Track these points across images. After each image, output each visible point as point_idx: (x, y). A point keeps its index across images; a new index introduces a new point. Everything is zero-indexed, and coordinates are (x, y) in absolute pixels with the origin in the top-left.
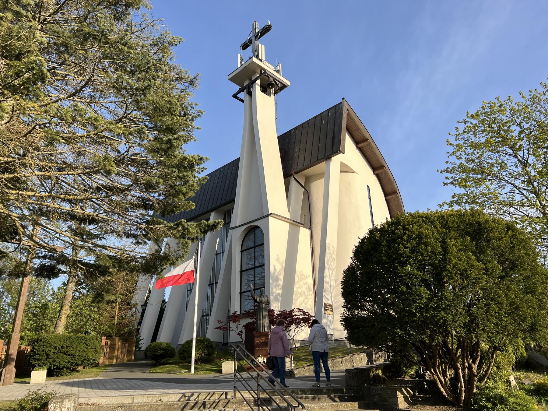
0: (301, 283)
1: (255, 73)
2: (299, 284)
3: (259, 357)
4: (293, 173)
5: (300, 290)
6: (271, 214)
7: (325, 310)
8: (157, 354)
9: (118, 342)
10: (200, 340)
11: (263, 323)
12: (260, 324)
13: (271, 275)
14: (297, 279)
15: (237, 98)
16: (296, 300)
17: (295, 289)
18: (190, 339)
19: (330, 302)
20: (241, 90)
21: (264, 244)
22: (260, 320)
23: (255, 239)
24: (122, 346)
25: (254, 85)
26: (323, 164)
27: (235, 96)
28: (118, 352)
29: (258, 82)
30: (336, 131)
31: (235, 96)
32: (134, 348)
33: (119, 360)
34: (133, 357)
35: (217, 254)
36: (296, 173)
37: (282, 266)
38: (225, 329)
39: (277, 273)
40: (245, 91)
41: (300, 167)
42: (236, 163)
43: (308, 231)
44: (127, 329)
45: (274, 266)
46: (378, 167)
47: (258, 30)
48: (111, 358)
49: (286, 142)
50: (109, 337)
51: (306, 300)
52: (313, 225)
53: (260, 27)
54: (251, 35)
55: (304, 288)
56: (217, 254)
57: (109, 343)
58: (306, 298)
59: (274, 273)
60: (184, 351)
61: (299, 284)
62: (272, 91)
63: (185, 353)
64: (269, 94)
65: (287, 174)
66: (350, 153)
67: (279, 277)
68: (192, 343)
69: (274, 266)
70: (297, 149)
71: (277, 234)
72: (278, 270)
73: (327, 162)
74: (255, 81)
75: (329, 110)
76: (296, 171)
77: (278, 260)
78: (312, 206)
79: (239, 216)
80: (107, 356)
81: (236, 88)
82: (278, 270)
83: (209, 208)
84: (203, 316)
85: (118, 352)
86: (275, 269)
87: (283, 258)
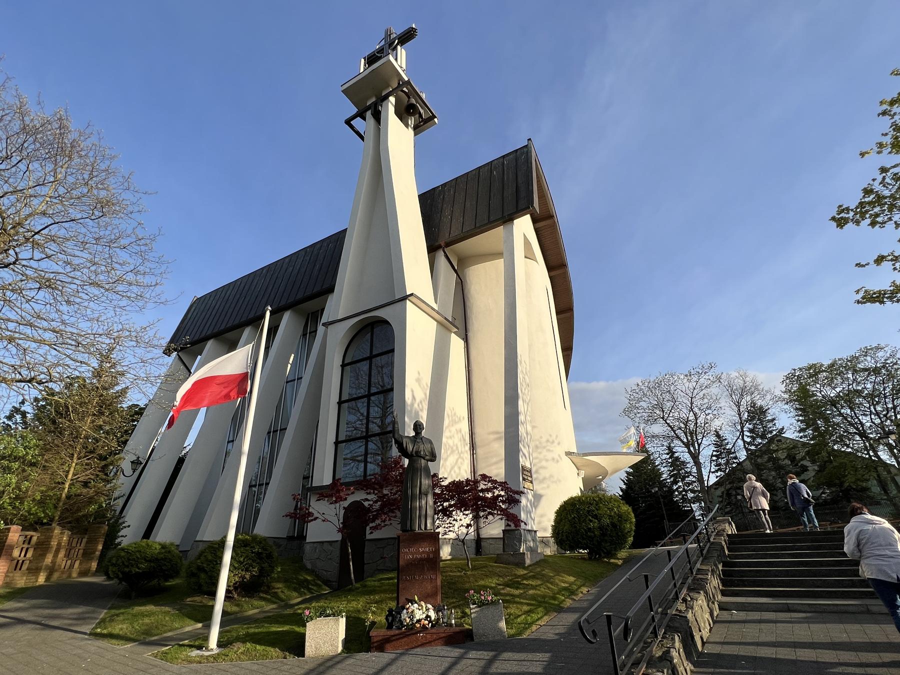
0: (453, 429)
1: (388, 86)
2: (450, 431)
3: (413, 602)
4: (443, 244)
5: (450, 442)
6: (412, 295)
7: (524, 479)
8: (135, 570)
9: (60, 536)
10: (243, 541)
11: (420, 507)
12: (412, 509)
13: (408, 408)
14: (446, 422)
15: (352, 127)
16: (446, 460)
17: (444, 440)
18: (218, 538)
19: (528, 465)
20: (361, 115)
21: (393, 351)
22: (413, 497)
23: (376, 342)
24: (70, 542)
25: (384, 104)
26: (500, 230)
27: (348, 122)
28: (56, 555)
29: (392, 99)
30: (520, 181)
31: (348, 122)
32: (100, 547)
33: (56, 576)
34: (94, 565)
35: (287, 382)
36: (448, 245)
37: (425, 394)
38: (300, 516)
39: (416, 405)
40: (369, 114)
41: (455, 232)
42: (337, 241)
43: (461, 343)
44: (93, 508)
45: (412, 391)
46: (557, 267)
47: (393, 36)
48: (34, 571)
49: (429, 202)
50: (30, 524)
51: (460, 460)
52: (470, 334)
53: (397, 31)
54: (383, 43)
55: (456, 440)
56: (287, 382)
57: (35, 539)
58: (460, 457)
59: (412, 405)
60: (201, 569)
61: (450, 431)
62: (411, 121)
63: (203, 576)
64: (407, 125)
65: (432, 249)
66: (524, 226)
67: (420, 413)
68: (222, 553)
69: (412, 391)
70: (447, 212)
71: (419, 333)
72: (418, 401)
73: (508, 226)
74: (386, 97)
75: (503, 157)
76: (448, 240)
77: (418, 380)
78: (467, 304)
79: (342, 304)
80: (25, 567)
81: (354, 110)
82: (418, 401)
83: (283, 303)
84: (251, 486)
85: (56, 555)
86: (414, 398)
87: (427, 379)
